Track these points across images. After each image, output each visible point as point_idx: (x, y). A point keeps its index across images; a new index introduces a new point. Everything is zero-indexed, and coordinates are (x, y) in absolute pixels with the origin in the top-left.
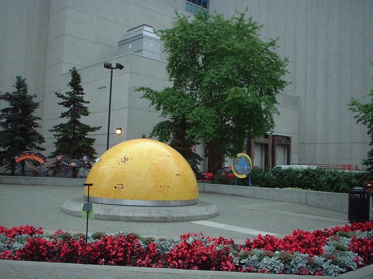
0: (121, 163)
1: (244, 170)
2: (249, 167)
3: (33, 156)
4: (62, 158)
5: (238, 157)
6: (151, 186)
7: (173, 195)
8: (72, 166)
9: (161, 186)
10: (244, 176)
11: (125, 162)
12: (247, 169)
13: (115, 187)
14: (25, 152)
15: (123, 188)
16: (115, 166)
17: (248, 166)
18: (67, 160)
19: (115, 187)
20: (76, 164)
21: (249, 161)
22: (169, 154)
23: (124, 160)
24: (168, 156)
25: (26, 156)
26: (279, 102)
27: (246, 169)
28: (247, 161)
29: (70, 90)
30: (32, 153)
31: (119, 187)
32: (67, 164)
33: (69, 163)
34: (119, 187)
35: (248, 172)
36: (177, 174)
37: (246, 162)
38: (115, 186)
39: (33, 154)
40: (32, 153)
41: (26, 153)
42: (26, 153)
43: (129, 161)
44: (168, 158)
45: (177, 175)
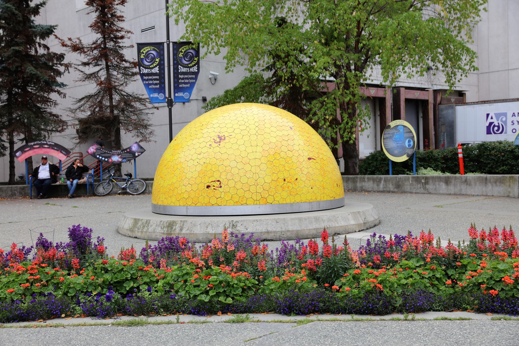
0: (214, 145)
1: (404, 148)
2: (412, 143)
3: (48, 150)
4: (97, 149)
5: (392, 127)
6: (268, 180)
7: (305, 194)
8: (114, 161)
9: (285, 180)
10: (404, 158)
11: (221, 144)
12: (409, 145)
13: (208, 187)
14: (32, 144)
15: (221, 187)
16: (204, 150)
17: (409, 141)
18: (105, 153)
19: (208, 187)
20: (121, 158)
21: (411, 132)
22: (291, 125)
23: (218, 140)
24: (291, 128)
25: (35, 150)
26: (39, 236)
27: (407, 146)
28: (407, 132)
29: (96, 37)
30: (45, 144)
31: (214, 186)
32: (106, 160)
33: (109, 157)
34: (214, 186)
35: (410, 152)
36: (308, 157)
37: (408, 135)
38: (207, 184)
39: (46, 146)
40: (45, 144)
41: (35, 145)
42: (35, 145)
43: (227, 140)
44: (291, 132)
45: (309, 159)
